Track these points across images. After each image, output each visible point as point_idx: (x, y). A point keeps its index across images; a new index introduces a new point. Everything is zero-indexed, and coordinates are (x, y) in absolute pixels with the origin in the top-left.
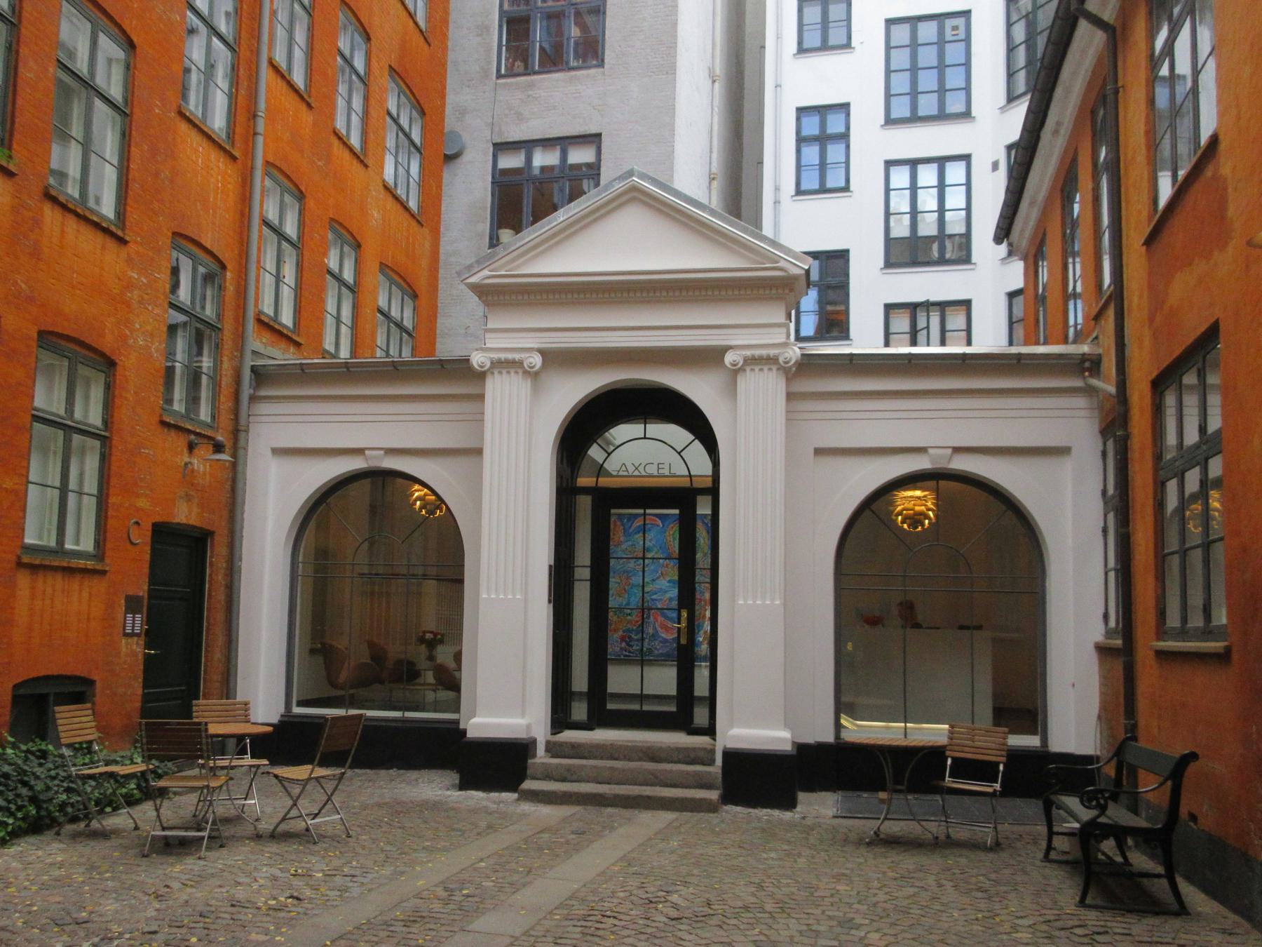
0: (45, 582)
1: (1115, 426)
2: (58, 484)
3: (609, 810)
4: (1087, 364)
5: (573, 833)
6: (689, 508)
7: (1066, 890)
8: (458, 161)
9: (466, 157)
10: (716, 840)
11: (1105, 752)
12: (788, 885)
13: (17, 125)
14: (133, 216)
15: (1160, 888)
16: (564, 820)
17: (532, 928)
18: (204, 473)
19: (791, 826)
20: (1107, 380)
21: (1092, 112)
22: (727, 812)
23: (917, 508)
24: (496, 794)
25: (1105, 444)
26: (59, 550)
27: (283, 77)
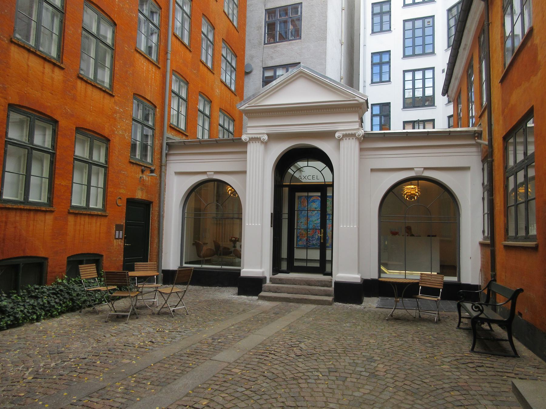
1: (487, 158)
2: (86, 184)
3: (291, 304)
4: (476, 135)
9: (253, 73)
12: (350, 340)
13: (64, 50)
14: (116, 86)
15: (507, 345)
16: (273, 308)
17: (239, 359)
18: (148, 181)
19: (359, 311)
20: (485, 140)
21: (479, 38)
25: (483, 166)
26: (87, 207)
27: (179, 40)
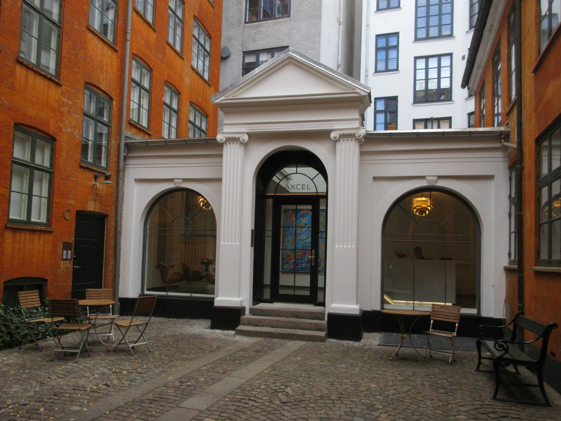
0: (20, 236)
1: (516, 166)
3: (275, 340)
4: (503, 136)
5: (254, 351)
6: (316, 204)
7: (485, 387)
8: (228, 60)
9: (232, 58)
10: (320, 356)
11: (508, 318)
12: (346, 384)
14: (64, 73)
15: (536, 391)
16: (253, 345)
18: (103, 189)
19: (357, 349)
20: (512, 143)
22: (329, 342)
23: (423, 206)
24: (226, 331)
25: (511, 174)
27: (141, 16)
